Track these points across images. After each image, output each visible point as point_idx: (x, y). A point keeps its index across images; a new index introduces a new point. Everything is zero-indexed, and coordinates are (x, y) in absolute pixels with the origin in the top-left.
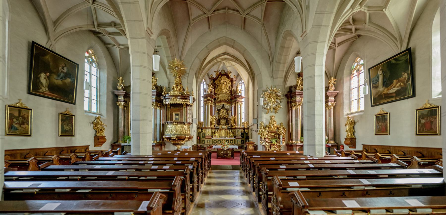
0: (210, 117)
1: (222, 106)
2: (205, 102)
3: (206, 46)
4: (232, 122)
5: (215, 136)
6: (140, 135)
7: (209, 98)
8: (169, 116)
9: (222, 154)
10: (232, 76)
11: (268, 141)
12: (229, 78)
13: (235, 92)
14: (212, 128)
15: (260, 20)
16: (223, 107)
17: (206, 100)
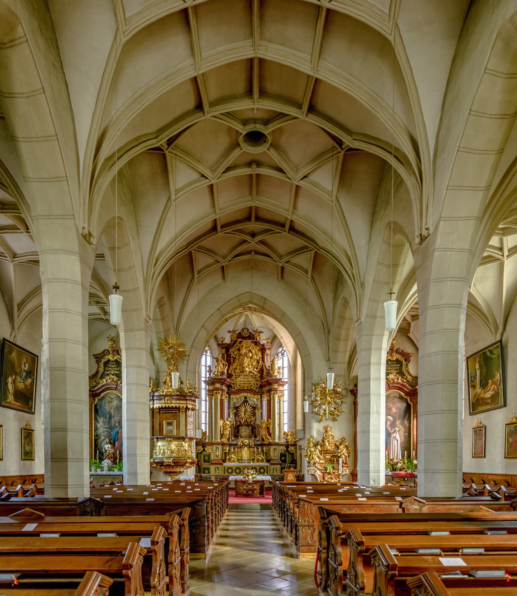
0: (220, 423)
1: (243, 399)
2: (211, 393)
3: (218, 309)
4: (264, 432)
5: (230, 460)
6: (138, 458)
7: (218, 385)
8: (157, 427)
9: (244, 489)
10: (263, 339)
11: (320, 468)
12: (256, 343)
13: (268, 374)
14: (223, 444)
15: (306, 272)
16: (246, 401)
17: (211, 388)
